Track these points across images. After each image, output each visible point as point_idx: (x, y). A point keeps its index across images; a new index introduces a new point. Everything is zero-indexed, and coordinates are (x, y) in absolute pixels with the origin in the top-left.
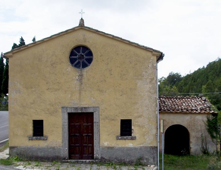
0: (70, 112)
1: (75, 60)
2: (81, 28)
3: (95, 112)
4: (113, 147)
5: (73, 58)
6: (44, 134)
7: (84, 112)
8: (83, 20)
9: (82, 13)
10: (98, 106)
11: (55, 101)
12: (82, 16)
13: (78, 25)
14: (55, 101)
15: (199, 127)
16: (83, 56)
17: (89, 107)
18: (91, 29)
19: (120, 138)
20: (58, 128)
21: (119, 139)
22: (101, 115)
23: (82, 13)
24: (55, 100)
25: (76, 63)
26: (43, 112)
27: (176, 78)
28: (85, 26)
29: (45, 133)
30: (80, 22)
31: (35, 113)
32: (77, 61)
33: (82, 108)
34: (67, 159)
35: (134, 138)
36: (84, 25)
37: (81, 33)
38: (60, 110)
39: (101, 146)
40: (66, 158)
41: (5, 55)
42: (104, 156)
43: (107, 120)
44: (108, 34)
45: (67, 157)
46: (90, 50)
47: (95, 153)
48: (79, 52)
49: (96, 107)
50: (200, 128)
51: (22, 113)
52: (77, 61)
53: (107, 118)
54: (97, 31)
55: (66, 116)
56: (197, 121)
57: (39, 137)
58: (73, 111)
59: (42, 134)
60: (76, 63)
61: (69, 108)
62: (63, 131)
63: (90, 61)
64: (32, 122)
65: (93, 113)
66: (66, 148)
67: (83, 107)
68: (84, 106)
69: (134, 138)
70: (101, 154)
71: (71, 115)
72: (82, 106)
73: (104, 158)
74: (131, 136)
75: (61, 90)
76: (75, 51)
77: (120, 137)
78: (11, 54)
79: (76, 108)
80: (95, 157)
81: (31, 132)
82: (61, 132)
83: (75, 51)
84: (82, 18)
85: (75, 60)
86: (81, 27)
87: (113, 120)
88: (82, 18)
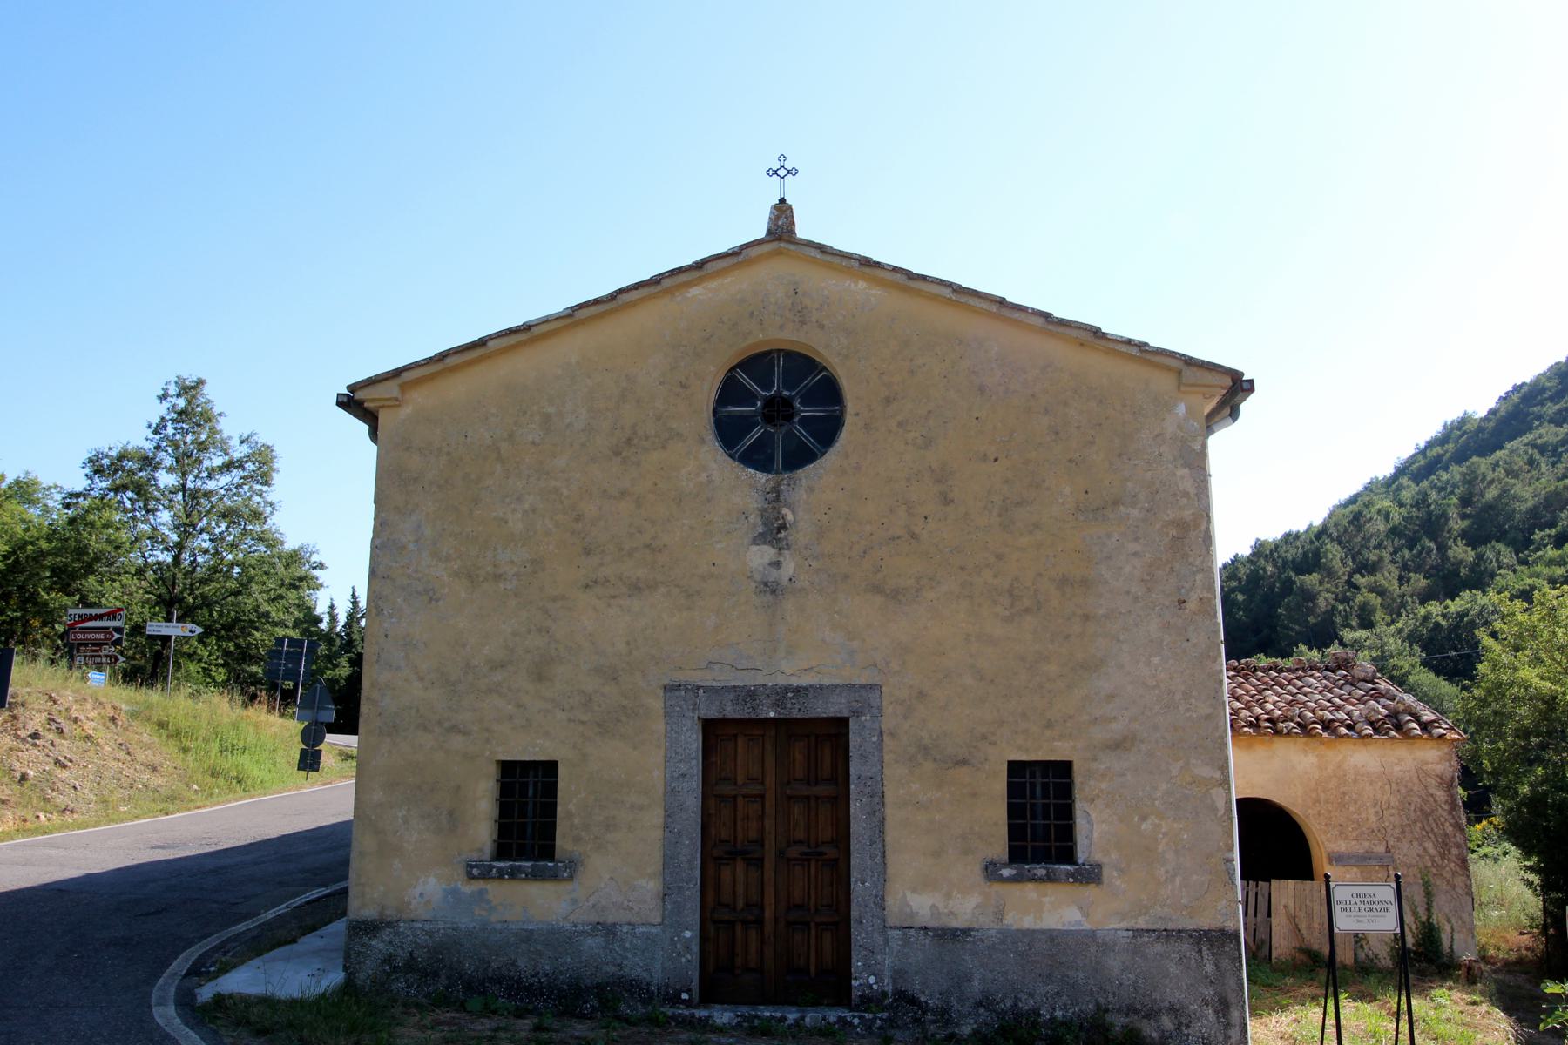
0: (713, 714)
1: (746, 424)
2: (779, 253)
3: (858, 713)
4: (966, 932)
5: (730, 416)
6: (559, 842)
7: (795, 714)
8: (790, 207)
9: (782, 172)
10: (876, 680)
11: (630, 653)
12: (783, 187)
13: (760, 232)
14: (630, 653)
15: (1372, 811)
16: (787, 403)
17: (821, 688)
18: (832, 254)
19: (1006, 872)
20: (641, 808)
21: (1002, 880)
22: (892, 735)
23: (782, 172)
24: (628, 643)
25: (749, 440)
26: (559, 715)
27: (608, 984)
28: (798, 236)
29: (563, 843)
30: (774, 220)
31: (511, 718)
32: (757, 433)
33: (782, 694)
34: (688, 1003)
35: (1090, 875)
36: (795, 233)
37: (773, 275)
38: (656, 704)
39: (890, 922)
40: (685, 996)
41: (359, 395)
42: (915, 986)
43: (928, 766)
44: (924, 278)
45: (689, 991)
46: (824, 368)
47: (857, 964)
48: (767, 385)
49: (863, 687)
50: (1373, 819)
51: (440, 723)
52: (757, 433)
53: (925, 750)
54: (866, 262)
55: (693, 741)
56: (1355, 781)
57: (528, 864)
58: (731, 712)
59: (546, 850)
60: (749, 440)
61: (707, 690)
62: (666, 827)
63: (827, 431)
64: (493, 771)
65: (841, 724)
66: (688, 934)
67: (786, 689)
68: (795, 682)
69: (1090, 875)
70: (894, 981)
71: (712, 730)
72: (782, 681)
73: (913, 1001)
74: (1075, 863)
75: (663, 590)
76: (743, 377)
77: (1004, 865)
78: (391, 389)
79: (749, 695)
80: (856, 993)
81: (482, 831)
82: (659, 833)
83: (743, 377)
84: (782, 201)
85: (746, 424)
86: (775, 245)
87: (964, 762)
88: (782, 201)
